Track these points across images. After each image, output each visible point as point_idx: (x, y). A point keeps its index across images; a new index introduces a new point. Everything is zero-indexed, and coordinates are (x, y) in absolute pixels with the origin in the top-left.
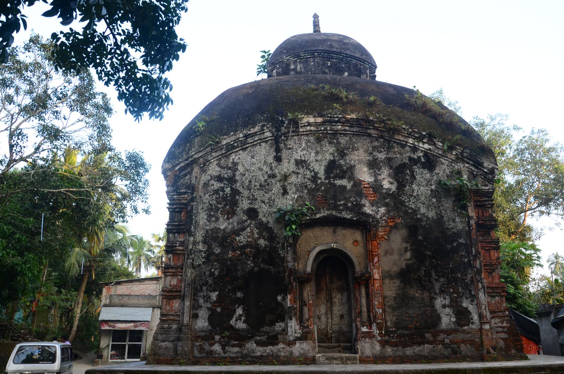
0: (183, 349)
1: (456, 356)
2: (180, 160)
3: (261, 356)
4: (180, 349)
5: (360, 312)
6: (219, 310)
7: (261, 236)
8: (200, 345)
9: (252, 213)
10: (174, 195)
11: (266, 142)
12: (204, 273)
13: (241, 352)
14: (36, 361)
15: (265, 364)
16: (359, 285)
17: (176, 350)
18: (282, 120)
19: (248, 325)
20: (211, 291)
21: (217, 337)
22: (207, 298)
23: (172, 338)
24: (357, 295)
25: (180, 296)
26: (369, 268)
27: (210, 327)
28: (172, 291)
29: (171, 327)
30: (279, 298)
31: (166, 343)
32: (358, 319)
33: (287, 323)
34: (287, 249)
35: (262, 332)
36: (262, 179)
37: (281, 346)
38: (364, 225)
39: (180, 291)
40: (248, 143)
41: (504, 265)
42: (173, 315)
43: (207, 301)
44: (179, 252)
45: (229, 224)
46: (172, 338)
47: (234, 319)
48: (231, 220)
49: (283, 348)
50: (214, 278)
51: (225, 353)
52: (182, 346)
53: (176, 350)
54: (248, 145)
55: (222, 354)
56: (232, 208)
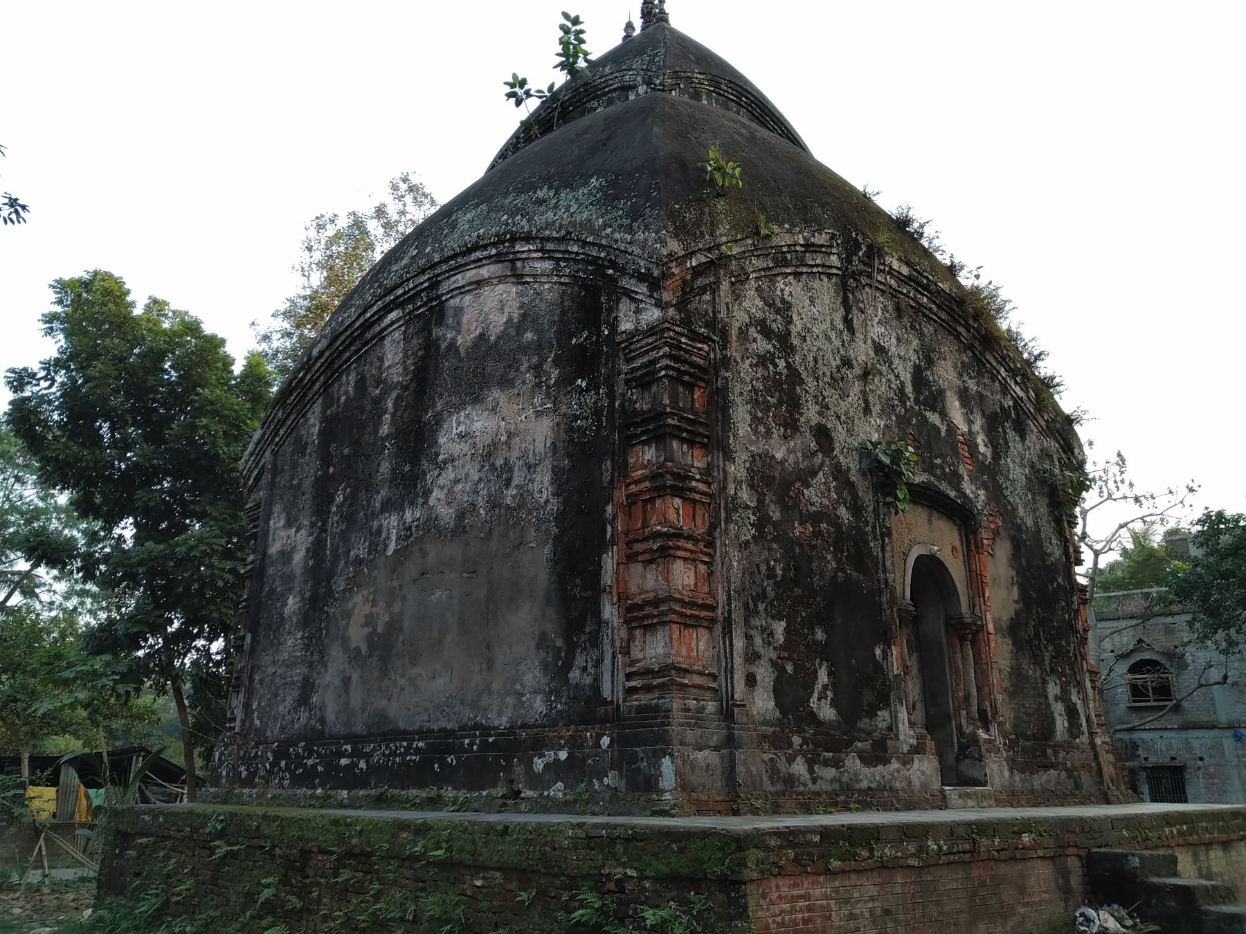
0: (748, 772)
1: (1075, 795)
2: (700, 245)
3: (870, 788)
4: (740, 769)
5: (967, 698)
6: (789, 668)
7: (841, 501)
8: (771, 760)
9: (823, 435)
10: (682, 335)
11: (829, 275)
12: (758, 566)
13: (839, 781)
14: (345, 807)
15: (886, 807)
16: (962, 639)
17: (730, 773)
18: (856, 239)
19: (839, 713)
20: (773, 618)
21: (797, 740)
22: (769, 635)
23: (715, 738)
24: (959, 661)
25: (713, 621)
26: (977, 608)
27: (778, 714)
28: (692, 605)
29: (704, 708)
30: (878, 652)
31: (706, 753)
32: (964, 713)
33: (896, 712)
34: (883, 541)
35: (861, 731)
36: (834, 364)
37: (895, 765)
38: (962, 516)
39: (713, 608)
40: (806, 265)
41: (374, 610)
42: (701, 674)
43: (769, 644)
44: (697, 497)
45: (789, 451)
46: (715, 738)
47: (816, 695)
48: (792, 444)
49: (898, 771)
50: (777, 585)
51: (814, 781)
52: (745, 763)
53: (730, 773)
54: (805, 270)
55: (810, 784)
56: (791, 415)
